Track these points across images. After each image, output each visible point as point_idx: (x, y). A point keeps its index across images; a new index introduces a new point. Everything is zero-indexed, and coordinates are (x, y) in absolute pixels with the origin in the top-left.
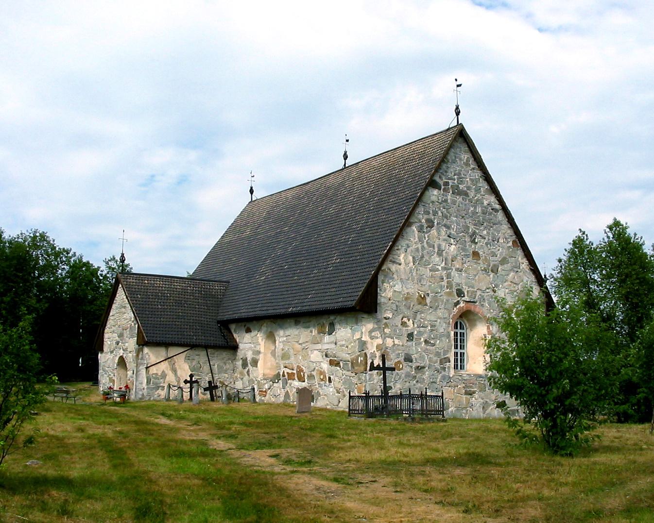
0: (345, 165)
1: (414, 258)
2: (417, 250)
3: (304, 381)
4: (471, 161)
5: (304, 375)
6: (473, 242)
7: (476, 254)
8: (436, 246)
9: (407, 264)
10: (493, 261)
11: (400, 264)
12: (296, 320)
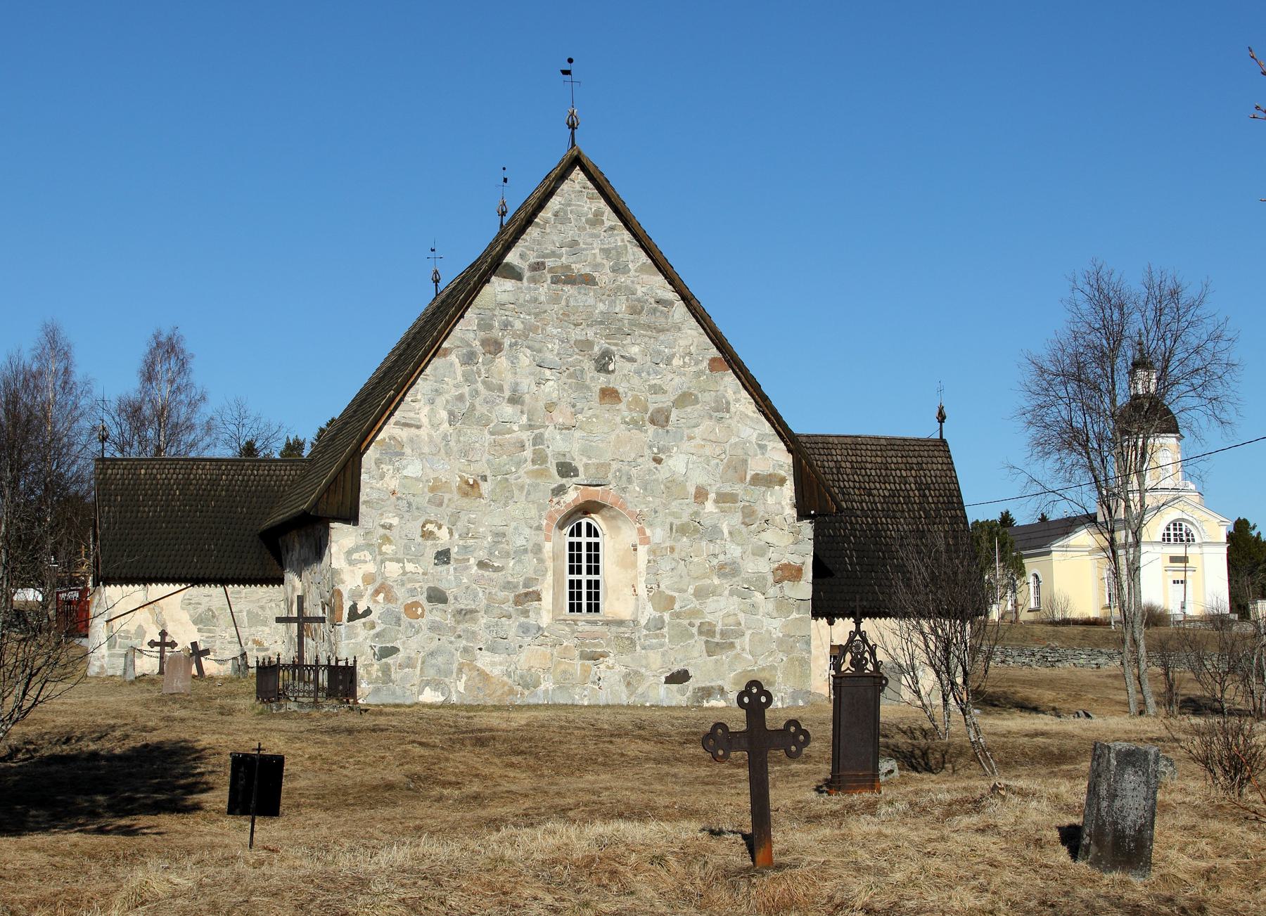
1: (451, 414)
2: (461, 398)
7: (609, 395)
9: (435, 426)
11: (418, 427)
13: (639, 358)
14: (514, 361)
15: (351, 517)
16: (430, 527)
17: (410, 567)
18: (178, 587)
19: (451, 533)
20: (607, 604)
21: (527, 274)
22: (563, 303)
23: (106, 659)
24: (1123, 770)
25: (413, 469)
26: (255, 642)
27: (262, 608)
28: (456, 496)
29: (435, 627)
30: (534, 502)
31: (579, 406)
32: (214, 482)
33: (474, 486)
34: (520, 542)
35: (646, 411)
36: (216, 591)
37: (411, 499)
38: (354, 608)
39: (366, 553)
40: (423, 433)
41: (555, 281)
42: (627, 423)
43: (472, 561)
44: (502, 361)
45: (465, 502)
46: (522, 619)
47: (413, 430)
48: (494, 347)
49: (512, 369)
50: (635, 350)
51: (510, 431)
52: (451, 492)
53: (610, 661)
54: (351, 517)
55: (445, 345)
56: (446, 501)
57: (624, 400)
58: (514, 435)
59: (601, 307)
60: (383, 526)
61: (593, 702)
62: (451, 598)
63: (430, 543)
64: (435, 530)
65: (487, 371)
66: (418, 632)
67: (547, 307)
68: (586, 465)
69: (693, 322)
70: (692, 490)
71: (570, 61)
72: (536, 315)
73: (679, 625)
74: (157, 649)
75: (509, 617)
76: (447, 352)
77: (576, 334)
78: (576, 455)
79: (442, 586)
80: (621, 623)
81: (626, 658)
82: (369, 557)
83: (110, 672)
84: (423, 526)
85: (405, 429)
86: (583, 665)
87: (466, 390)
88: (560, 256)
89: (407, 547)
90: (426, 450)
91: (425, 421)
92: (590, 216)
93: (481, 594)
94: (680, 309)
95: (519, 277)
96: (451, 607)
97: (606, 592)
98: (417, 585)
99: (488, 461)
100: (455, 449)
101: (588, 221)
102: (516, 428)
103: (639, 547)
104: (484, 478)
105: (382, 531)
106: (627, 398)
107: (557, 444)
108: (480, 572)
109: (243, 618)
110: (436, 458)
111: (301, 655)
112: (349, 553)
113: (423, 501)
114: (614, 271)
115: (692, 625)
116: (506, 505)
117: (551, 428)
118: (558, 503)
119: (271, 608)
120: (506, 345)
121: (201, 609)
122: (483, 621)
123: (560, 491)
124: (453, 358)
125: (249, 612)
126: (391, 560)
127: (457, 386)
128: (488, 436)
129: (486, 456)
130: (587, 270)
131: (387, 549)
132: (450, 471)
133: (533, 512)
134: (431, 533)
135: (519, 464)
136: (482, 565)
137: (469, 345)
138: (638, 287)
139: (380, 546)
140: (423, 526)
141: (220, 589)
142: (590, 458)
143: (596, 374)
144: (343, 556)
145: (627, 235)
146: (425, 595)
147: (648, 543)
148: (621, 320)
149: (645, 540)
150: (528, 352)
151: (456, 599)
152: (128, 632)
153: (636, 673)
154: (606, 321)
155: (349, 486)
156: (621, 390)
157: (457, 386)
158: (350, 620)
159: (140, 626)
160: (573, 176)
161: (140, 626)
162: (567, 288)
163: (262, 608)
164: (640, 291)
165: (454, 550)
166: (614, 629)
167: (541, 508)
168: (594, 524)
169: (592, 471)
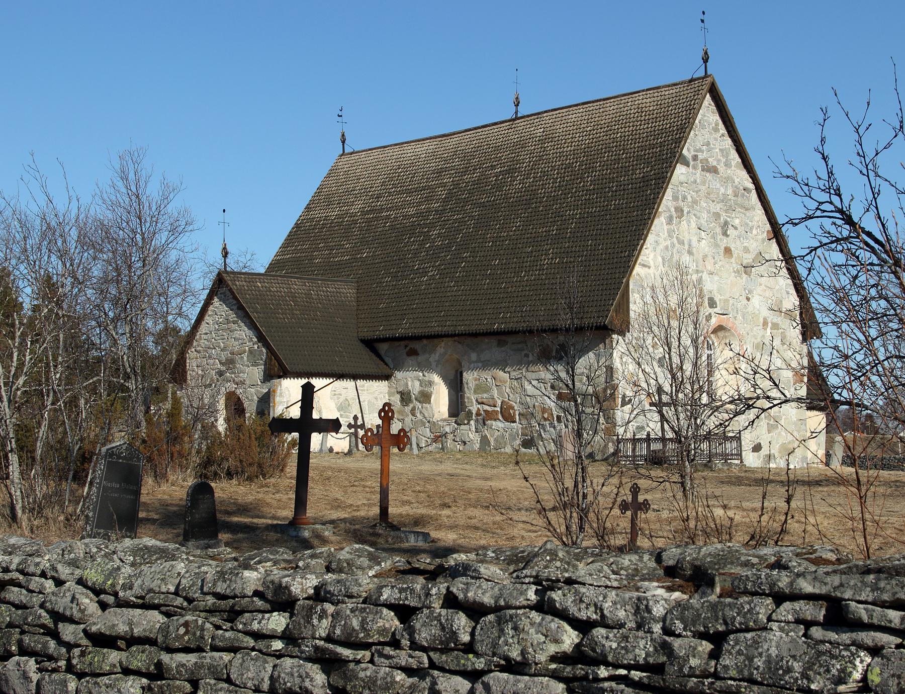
0: (516, 113)
1: (663, 259)
2: (667, 248)
3: (515, 422)
4: (721, 126)
5: (514, 413)
6: (725, 234)
7: (728, 251)
8: (686, 242)
9: (656, 267)
10: (748, 259)
11: (649, 267)
12: (499, 341)
18: (328, 381)
21: (692, 163)
24: (639, 548)
36: (349, 384)
40: (651, 271)
44: (684, 223)
47: (647, 269)
49: (687, 228)
50: (737, 222)
54: (622, 333)
59: (722, 190)
67: (700, 187)
68: (720, 300)
70: (761, 320)
72: (697, 192)
78: (715, 292)
91: (652, 264)
94: (754, 195)
114: (726, 165)
120: (685, 212)
121: (342, 399)
125: (369, 402)
130: (715, 164)
137: (670, 211)
154: (724, 200)
163: (376, 398)
169: (722, 304)
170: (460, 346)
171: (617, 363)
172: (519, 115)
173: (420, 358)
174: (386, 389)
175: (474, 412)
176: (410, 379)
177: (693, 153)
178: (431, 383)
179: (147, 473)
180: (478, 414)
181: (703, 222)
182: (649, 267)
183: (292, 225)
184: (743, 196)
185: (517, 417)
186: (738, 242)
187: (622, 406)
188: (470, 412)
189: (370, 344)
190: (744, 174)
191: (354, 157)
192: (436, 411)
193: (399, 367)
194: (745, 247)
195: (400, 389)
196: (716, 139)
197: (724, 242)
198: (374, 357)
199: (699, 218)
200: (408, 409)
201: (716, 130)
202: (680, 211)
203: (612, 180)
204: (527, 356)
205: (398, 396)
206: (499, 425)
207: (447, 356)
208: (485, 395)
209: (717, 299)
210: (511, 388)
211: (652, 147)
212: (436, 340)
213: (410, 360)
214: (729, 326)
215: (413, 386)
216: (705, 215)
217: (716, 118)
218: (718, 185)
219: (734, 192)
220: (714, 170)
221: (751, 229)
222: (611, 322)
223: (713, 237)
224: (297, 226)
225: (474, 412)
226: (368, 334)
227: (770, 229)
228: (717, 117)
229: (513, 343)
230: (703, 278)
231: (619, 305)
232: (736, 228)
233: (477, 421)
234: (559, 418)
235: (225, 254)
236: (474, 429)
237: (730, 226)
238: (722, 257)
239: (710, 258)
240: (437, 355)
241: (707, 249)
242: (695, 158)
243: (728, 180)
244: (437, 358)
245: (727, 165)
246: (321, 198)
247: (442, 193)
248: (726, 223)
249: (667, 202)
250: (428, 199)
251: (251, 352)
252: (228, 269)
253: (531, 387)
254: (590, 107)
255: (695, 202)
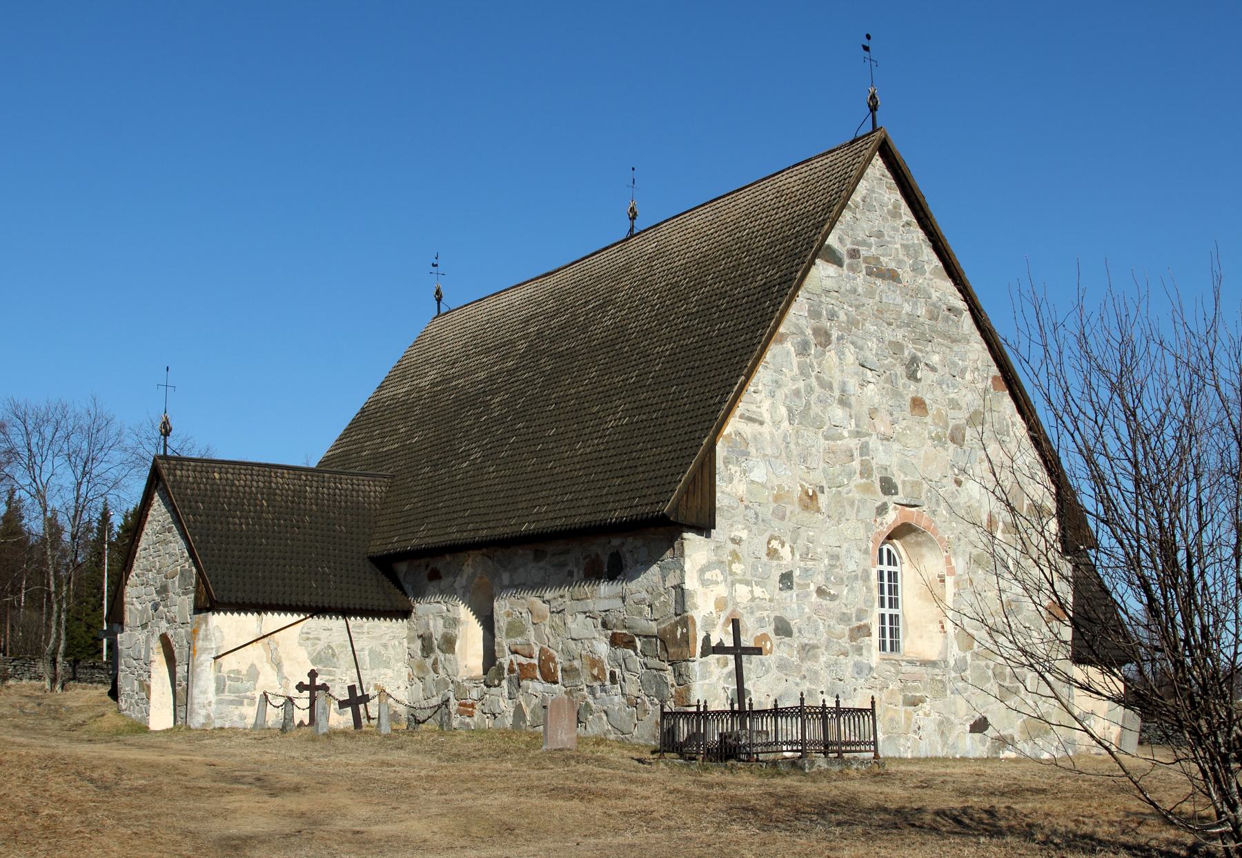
1: (790, 410)
2: (797, 393)
3: (556, 682)
5: (555, 668)
6: (912, 376)
8: (835, 386)
9: (777, 424)
11: (762, 423)
12: (536, 551)
13: (939, 367)
14: (841, 355)
15: (705, 527)
16: (775, 544)
17: (758, 591)
18: (296, 618)
19: (793, 552)
20: (907, 640)
21: (847, 261)
22: (877, 298)
23: (214, 706)
25: (759, 473)
26: (376, 687)
27: (385, 646)
28: (797, 509)
29: (783, 666)
30: (862, 521)
31: (896, 414)
32: (300, 493)
33: (813, 498)
34: (852, 567)
35: (947, 427)
36: (336, 624)
37: (758, 509)
38: (707, 639)
39: (718, 571)
40: (766, 429)
41: (869, 273)
42: (932, 438)
43: (812, 587)
44: (831, 355)
45: (805, 516)
46: (857, 658)
47: (756, 426)
48: (823, 338)
49: (838, 364)
50: (935, 359)
51: (841, 437)
52: (792, 503)
53: (926, 706)
54: (705, 527)
55: (782, 329)
56: (788, 514)
57: (930, 412)
58: (844, 441)
59: (907, 308)
60: (733, 540)
61: (916, 755)
62: (795, 630)
63: (775, 563)
64: (779, 547)
65: (820, 365)
66: (767, 672)
67: (864, 300)
68: (904, 482)
69: (978, 333)
71: (868, 37)
72: (857, 307)
73: (978, 666)
74: (307, 693)
75: (846, 654)
76: (782, 339)
77: (891, 334)
78: (895, 469)
79: (787, 615)
80: (934, 664)
81: (939, 704)
82: (721, 578)
83: (218, 724)
84: (769, 543)
85: (750, 424)
86: (906, 711)
87: (801, 384)
88: (870, 246)
89: (754, 567)
90: (769, 451)
91: (766, 416)
92: (890, 207)
93: (821, 627)
94: (967, 320)
95: (839, 263)
96: (796, 641)
97: (906, 629)
98: (765, 613)
99: (824, 470)
100: (795, 453)
101: (889, 211)
102: (846, 434)
103: (947, 579)
104: (822, 490)
105: (731, 546)
106: (932, 411)
107: (884, 457)
108: (819, 600)
109: (364, 657)
110: (779, 461)
111: (741, 692)
112: (702, 571)
113: (767, 512)
114: (913, 270)
115: (987, 666)
116: (839, 522)
117: (874, 437)
118: (881, 524)
119: (394, 646)
120: (834, 338)
121: (321, 645)
122: (823, 659)
123: (882, 510)
124: (789, 346)
125: (371, 651)
126: (741, 582)
127: (794, 379)
128: (822, 441)
129: (822, 465)
130: (893, 265)
131: (737, 568)
132: (792, 479)
133: (861, 533)
134: (776, 551)
135: (850, 475)
136: (820, 592)
137: (803, 333)
138: (932, 291)
139: (731, 563)
140: (769, 543)
141: (341, 622)
142: (906, 475)
143: (908, 382)
144: (696, 575)
145: (921, 234)
146: (773, 626)
147: (954, 574)
148: (922, 324)
149: (951, 571)
150: (852, 347)
151: (800, 632)
152: (238, 672)
153: (948, 720)
154: (911, 322)
155: (707, 488)
156: (927, 402)
157: (794, 379)
158: (703, 654)
159: (253, 666)
160: (874, 161)
161: (253, 666)
162: (879, 282)
163: (385, 646)
164: (935, 296)
165: (797, 573)
166: (930, 670)
167: (868, 528)
168: (893, 551)
169: (908, 489)
170: (490, 563)
171: (691, 584)
172: (635, 231)
173: (444, 583)
174: (405, 632)
175: (506, 667)
176: (432, 611)
177: (849, 246)
178: (455, 622)
179: (1225, 672)
180: (511, 670)
181: (871, 357)
182: (762, 423)
183: (358, 410)
184: (947, 319)
185: (559, 674)
186: (938, 392)
187: (703, 654)
188: (501, 667)
189: (385, 564)
190: (948, 286)
191: (448, 317)
192: (461, 664)
193: (420, 594)
194: (951, 401)
195: (421, 633)
196: (896, 229)
197: (912, 389)
198: (387, 583)
199: (861, 349)
200: (429, 662)
201: (895, 214)
202: (823, 338)
203: (722, 296)
204: (571, 574)
205: (419, 642)
206: (537, 686)
207: (476, 580)
208: (519, 640)
209: (898, 479)
210: (552, 627)
211: (785, 239)
212: (461, 555)
213: (431, 586)
214: (922, 525)
215: (435, 626)
216: (872, 344)
217: (894, 196)
218: (899, 300)
219: (930, 312)
220: (892, 276)
221: (963, 372)
222: (676, 508)
223: (891, 380)
224: (363, 410)
225: (506, 667)
226: (377, 547)
227: (998, 374)
228: (897, 195)
229: (553, 555)
230: (871, 445)
231: (693, 480)
232: (933, 369)
233: (510, 681)
234: (613, 674)
235: (166, 431)
236: (506, 694)
237: (922, 365)
238: (907, 414)
239: (883, 413)
240: (465, 577)
241: (877, 399)
242: (854, 254)
243: (917, 293)
244: (464, 582)
245: (917, 269)
246: (400, 372)
247: (522, 346)
248: (914, 360)
249: (797, 315)
250: (504, 358)
251: (182, 573)
252: (169, 453)
253: (566, 620)
254: (721, 202)
255: (853, 322)
